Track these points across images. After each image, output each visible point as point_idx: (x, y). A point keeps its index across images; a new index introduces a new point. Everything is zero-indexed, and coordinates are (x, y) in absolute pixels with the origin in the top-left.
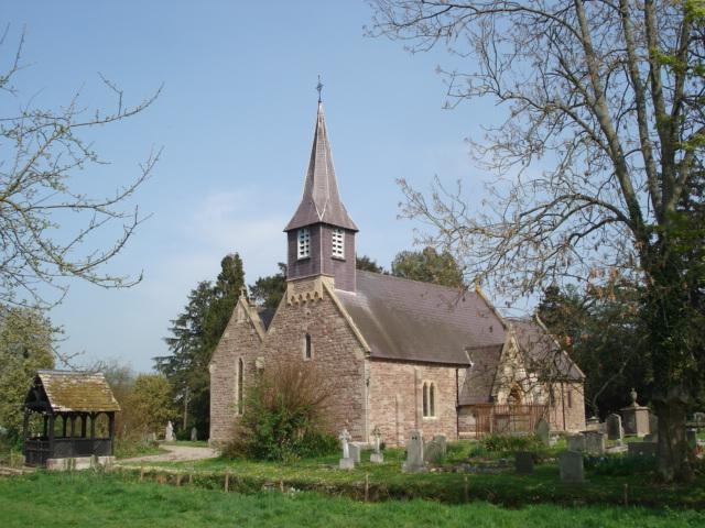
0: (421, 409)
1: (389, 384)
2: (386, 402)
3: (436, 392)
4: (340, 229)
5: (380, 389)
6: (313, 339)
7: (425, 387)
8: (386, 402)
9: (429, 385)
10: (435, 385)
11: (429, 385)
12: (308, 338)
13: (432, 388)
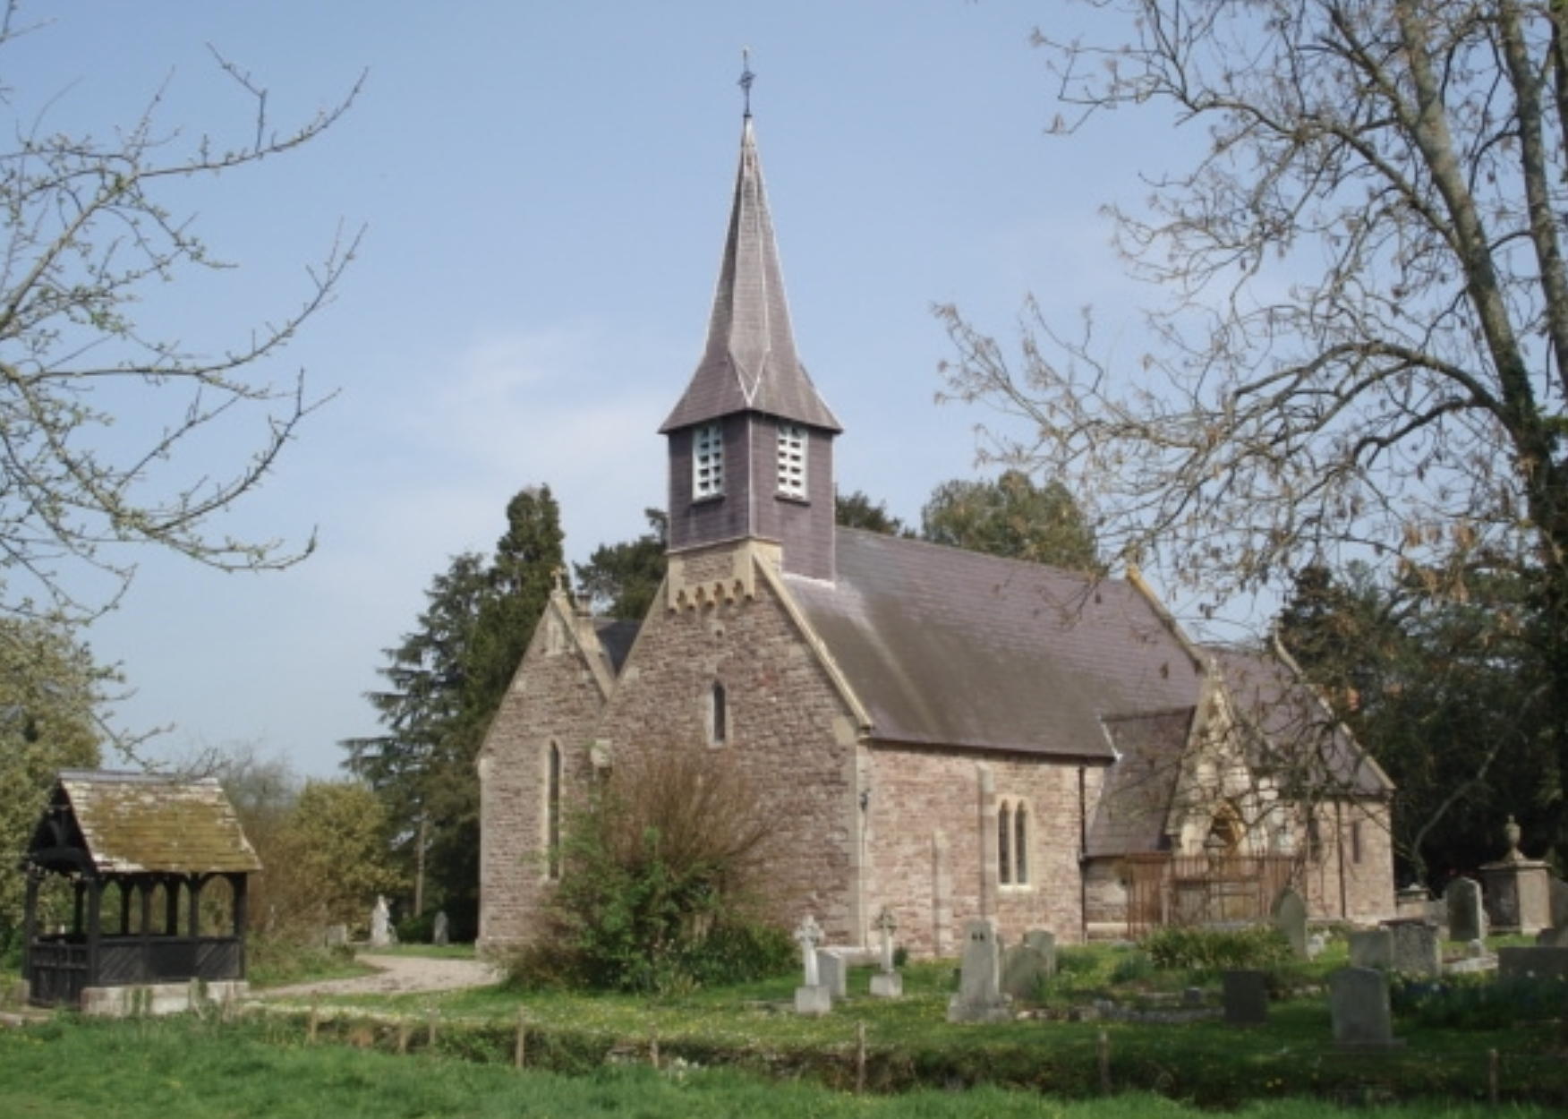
0: (994, 867)
1: (914, 804)
2: (908, 848)
3: (1031, 824)
4: (797, 427)
5: (894, 817)
6: (732, 696)
7: (1004, 814)
8: (908, 848)
9: (1013, 808)
10: (1029, 808)
11: (1013, 808)
12: (719, 693)
13: (1021, 815)
